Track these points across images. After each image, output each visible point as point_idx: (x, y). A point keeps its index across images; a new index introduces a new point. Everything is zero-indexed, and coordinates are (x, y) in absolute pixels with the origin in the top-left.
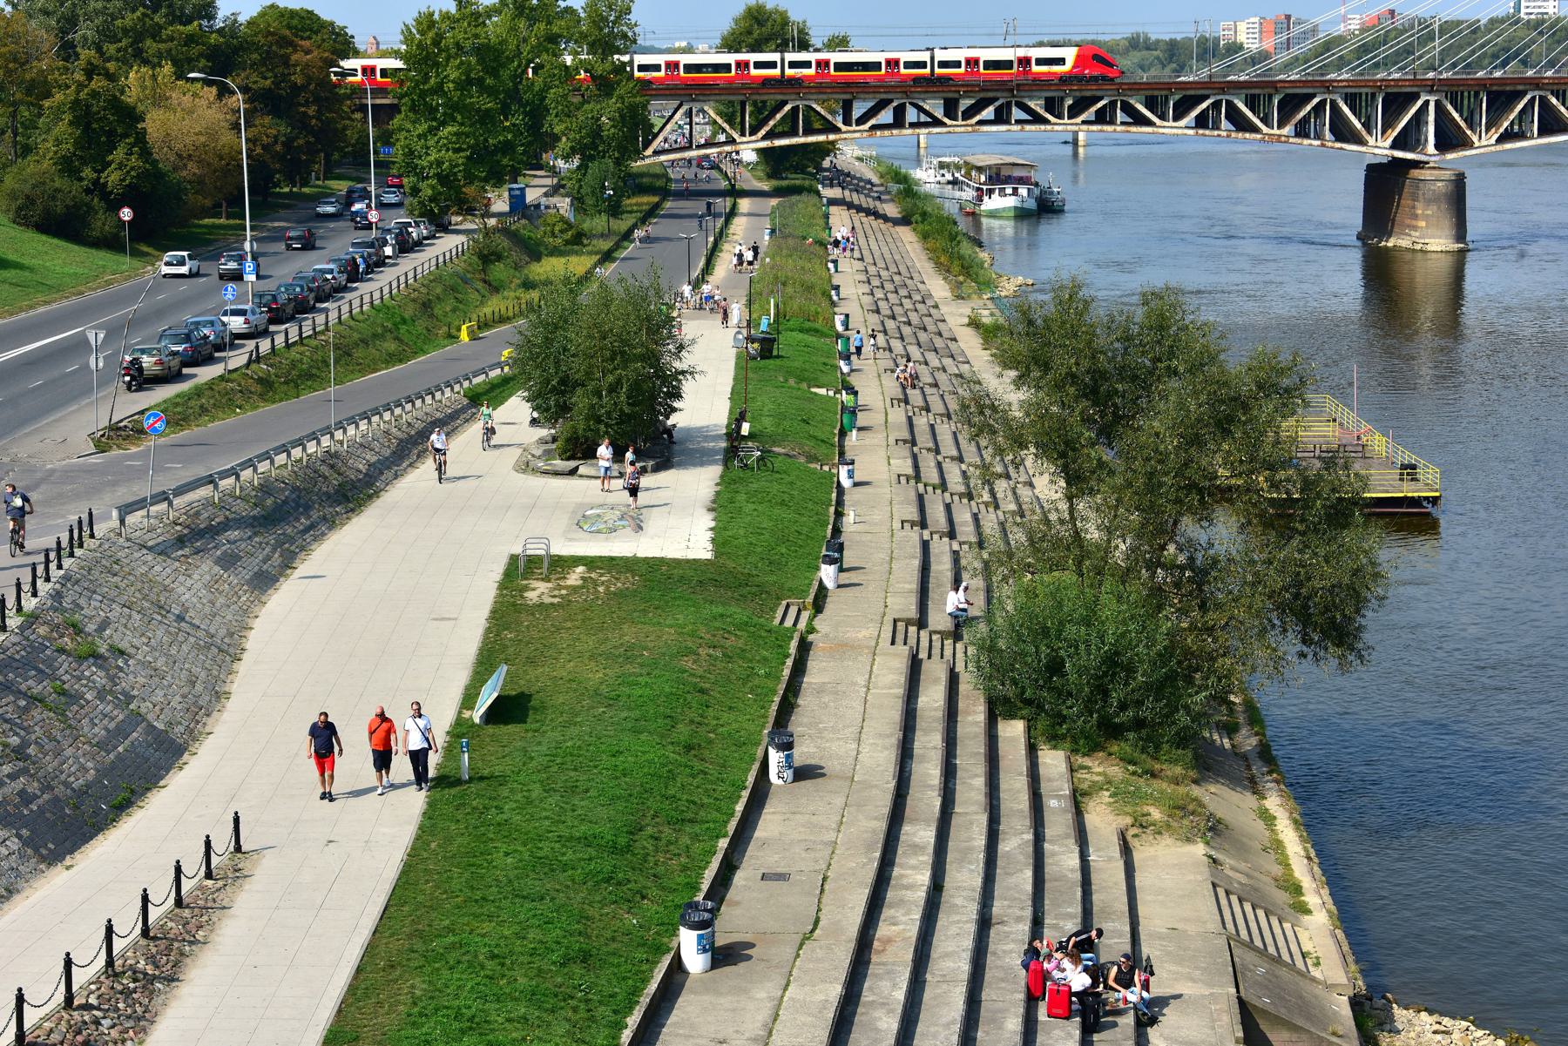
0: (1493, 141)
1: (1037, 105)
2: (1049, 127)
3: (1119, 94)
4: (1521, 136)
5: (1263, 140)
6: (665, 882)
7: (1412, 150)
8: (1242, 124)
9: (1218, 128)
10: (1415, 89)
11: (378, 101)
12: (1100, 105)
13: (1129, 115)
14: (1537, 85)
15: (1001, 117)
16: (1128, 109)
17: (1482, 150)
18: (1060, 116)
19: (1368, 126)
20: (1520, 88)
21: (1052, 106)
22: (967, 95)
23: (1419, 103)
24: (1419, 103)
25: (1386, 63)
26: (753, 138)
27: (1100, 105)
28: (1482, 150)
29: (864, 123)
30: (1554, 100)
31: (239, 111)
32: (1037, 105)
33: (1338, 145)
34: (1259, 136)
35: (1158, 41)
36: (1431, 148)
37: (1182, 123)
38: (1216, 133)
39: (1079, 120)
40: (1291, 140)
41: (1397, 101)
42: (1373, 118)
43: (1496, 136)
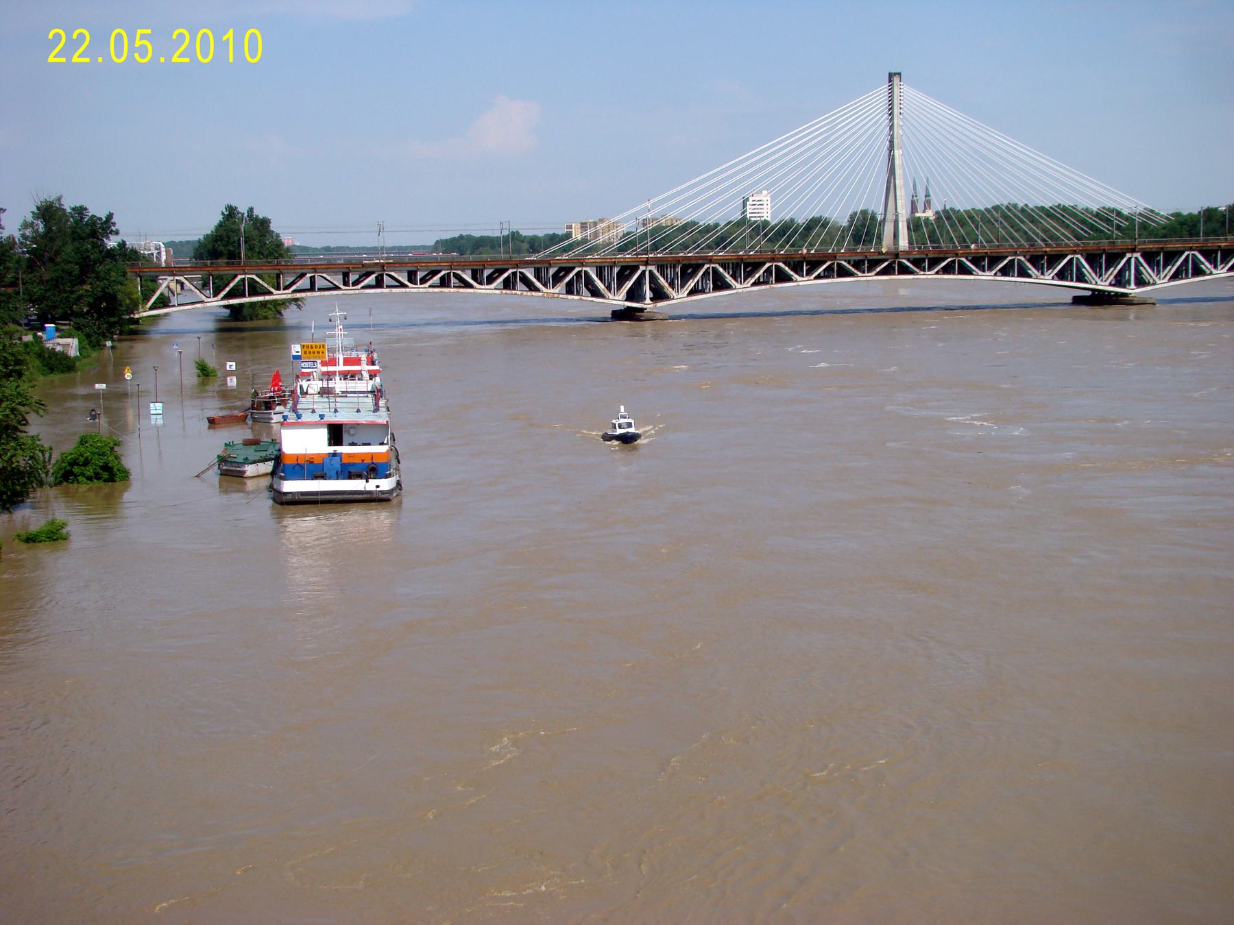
0: (685, 295)
1: (467, 277)
2: (408, 290)
3: (451, 269)
4: (703, 291)
5: (543, 296)
6: (135, 274)
7: (638, 302)
8: (531, 287)
9: (514, 289)
10: (636, 264)
11: (1201, 234)
12: (506, 275)
13: (463, 283)
14: (711, 260)
15: (379, 283)
16: (525, 280)
17: (679, 301)
18: (481, 283)
19: (609, 288)
20: (700, 262)
21: (412, 277)
22: (355, 270)
23: (639, 273)
24: (639, 273)
25: (685, 247)
26: (215, 299)
27: (506, 275)
28: (679, 301)
29: (288, 289)
30: (721, 270)
31: (962, 226)
32: (467, 277)
33: (529, 293)
34: (540, 294)
35: (334, 248)
36: (648, 301)
37: (493, 286)
38: (514, 292)
39: (427, 285)
40: (561, 296)
41: (626, 272)
42: (191, 273)
43: (687, 292)
